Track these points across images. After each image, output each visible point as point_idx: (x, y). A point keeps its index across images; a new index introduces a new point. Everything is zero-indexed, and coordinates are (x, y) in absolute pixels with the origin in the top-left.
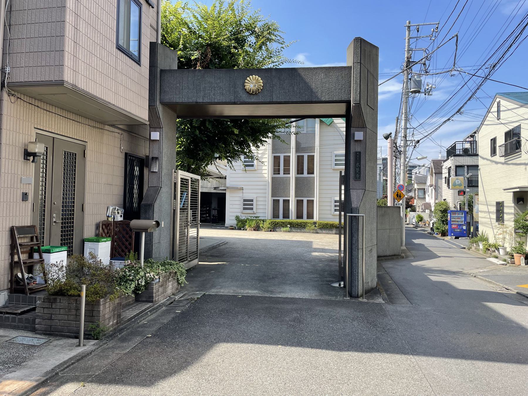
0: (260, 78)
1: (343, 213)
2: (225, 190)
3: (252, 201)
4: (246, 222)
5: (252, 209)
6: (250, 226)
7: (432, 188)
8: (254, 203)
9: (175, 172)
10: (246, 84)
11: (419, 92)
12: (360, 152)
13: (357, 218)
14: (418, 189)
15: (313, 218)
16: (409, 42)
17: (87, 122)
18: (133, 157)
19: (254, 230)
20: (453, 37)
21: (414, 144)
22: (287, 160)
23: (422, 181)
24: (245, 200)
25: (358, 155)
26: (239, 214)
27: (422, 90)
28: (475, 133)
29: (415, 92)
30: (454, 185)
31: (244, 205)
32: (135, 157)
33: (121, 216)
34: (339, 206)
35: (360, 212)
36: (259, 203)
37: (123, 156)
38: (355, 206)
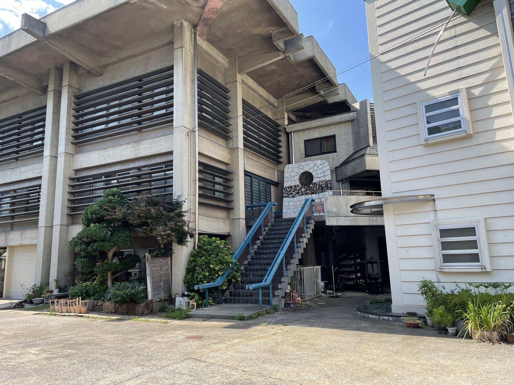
3: (471, 231)
4: (464, 306)
5: (475, 258)
6: (482, 324)
8: (481, 236)
19: (504, 339)
24: (444, 233)
26: (431, 277)
31: (445, 246)
36: (499, 237)
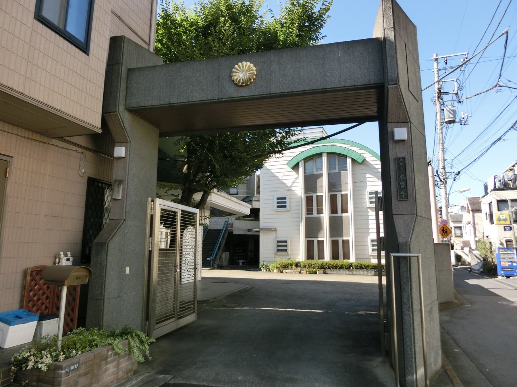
0: (252, 65)
1: (383, 253)
2: (259, 232)
5: (286, 250)
7: (470, 225)
9: (153, 201)
10: (234, 74)
11: (453, 122)
12: (404, 159)
13: (408, 260)
14: (455, 227)
15: (349, 258)
16: (438, 73)
17: (15, 130)
18: (102, 183)
20: (503, 34)
21: (453, 176)
22: (320, 199)
23: (458, 219)
24: (278, 242)
25: (402, 164)
27: (457, 120)
28: (514, 166)
29: (450, 122)
30: (499, 220)
31: (278, 246)
32: (105, 184)
33: (68, 260)
34: (377, 245)
35: (412, 250)
37: (85, 181)
38: (404, 241)
